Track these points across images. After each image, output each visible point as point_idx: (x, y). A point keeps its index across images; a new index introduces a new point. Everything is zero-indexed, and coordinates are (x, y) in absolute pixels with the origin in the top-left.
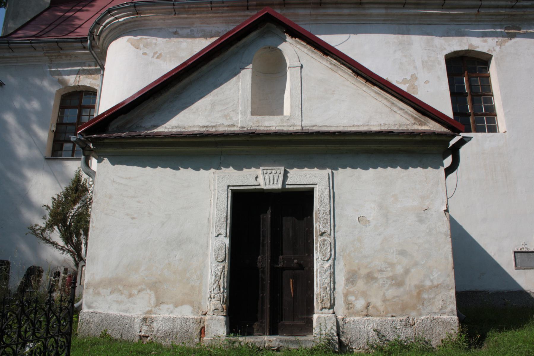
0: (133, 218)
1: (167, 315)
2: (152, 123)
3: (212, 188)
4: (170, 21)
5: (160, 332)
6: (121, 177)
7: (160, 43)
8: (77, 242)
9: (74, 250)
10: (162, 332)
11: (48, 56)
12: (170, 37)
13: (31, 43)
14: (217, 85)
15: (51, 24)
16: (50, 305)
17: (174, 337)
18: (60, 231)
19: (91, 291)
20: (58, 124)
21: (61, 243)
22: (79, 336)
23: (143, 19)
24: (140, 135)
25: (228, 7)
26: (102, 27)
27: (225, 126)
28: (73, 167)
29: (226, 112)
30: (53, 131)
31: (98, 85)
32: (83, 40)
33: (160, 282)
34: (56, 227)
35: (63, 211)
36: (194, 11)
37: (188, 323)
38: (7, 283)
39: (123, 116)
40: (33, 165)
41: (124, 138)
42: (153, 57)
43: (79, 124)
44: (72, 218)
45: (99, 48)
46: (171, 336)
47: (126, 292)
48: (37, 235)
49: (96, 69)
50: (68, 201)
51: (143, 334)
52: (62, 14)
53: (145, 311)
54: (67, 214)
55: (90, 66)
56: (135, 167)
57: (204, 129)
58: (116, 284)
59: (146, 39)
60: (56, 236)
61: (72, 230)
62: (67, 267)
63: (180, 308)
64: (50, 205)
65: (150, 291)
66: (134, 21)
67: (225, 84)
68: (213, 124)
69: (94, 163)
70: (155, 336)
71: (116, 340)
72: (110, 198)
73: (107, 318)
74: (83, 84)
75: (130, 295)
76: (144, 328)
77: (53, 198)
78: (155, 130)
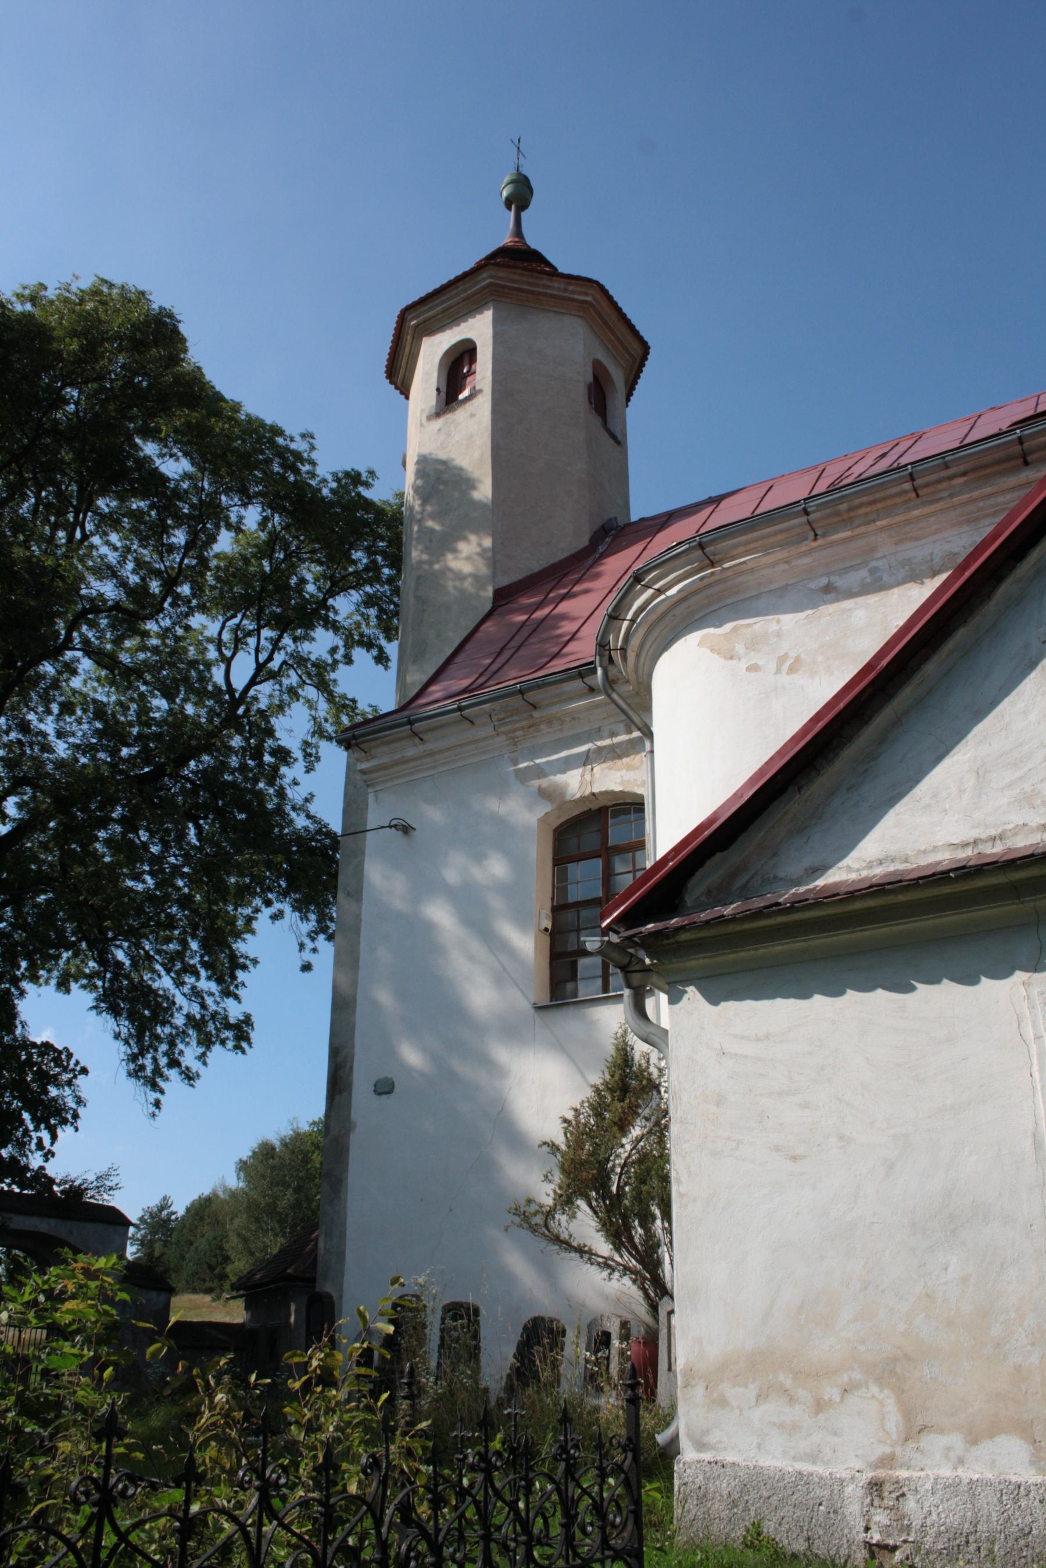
0: (794, 1158)
1: (946, 1472)
2: (807, 862)
3: (1030, 1034)
4: (807, 560)
5: (932, 1532)
6: (743, 1038)
7: (790, 628)
8: (646, 1241)
9: (639, 1267)
10: (939, 1534)
11: (505, 733)
12: (814, 606)
13: (460, 709)
14: (979, 713)
15: (502, 649)
16: (567, 1460)
17: (983, 1553)
18: (595, 1212)
19: (699, 1392)
20: (555, 910)
21: (603, 1247)
22: (680, 1539)
23: (729, 573)
24: (778, 904)
25: (964, 474)
26: (626, 624)
27: (1033, 831)
28: (612, 1018)
29: (1027, 787)
30: (546, 930)
31: (644, 783)
32: (585, 671)
33: (907, 1357)
34: (581, 1203)
35: (593, 1154)
36: (866, 514)
37: (1023, 1503)
38: (477, 1371)
39: (718, 856)
40: (513, 1032)
41: (733, 919)
42: (778, 671)
43: (601, 904)
44: (621, 1173)
45: (628, 682)
46: (973, 1547)
47: (802, 1393)
48: (533, 1229)
49: (631, 741)
50: (607, 1123)
51: (876, 1537)
52: (524, 618)
53: (873, 1458)
54: (608, 1160)
55: (613, 734)
56: (779, 1002)
57: (969, 852)
58: (764, 1371)
59: (749, 625)
60: (584, 1224)
61: (626, 1208)
62: (627, 1316)
63: (986, 1448)
64: (560, 1140)
65: (881, 1391)
66: (709, 586)
67: (1006, 702)
68: (993, 832)
69: (658, 1005)
70: (917, 1546)
71: (795, 1556)
72: (718, 1104)
73: (754, 1481)
74: (604, 789)
75: (820, 1406)
76: (876, 1518)
77: (565, 1121)
78: (820, 883)
